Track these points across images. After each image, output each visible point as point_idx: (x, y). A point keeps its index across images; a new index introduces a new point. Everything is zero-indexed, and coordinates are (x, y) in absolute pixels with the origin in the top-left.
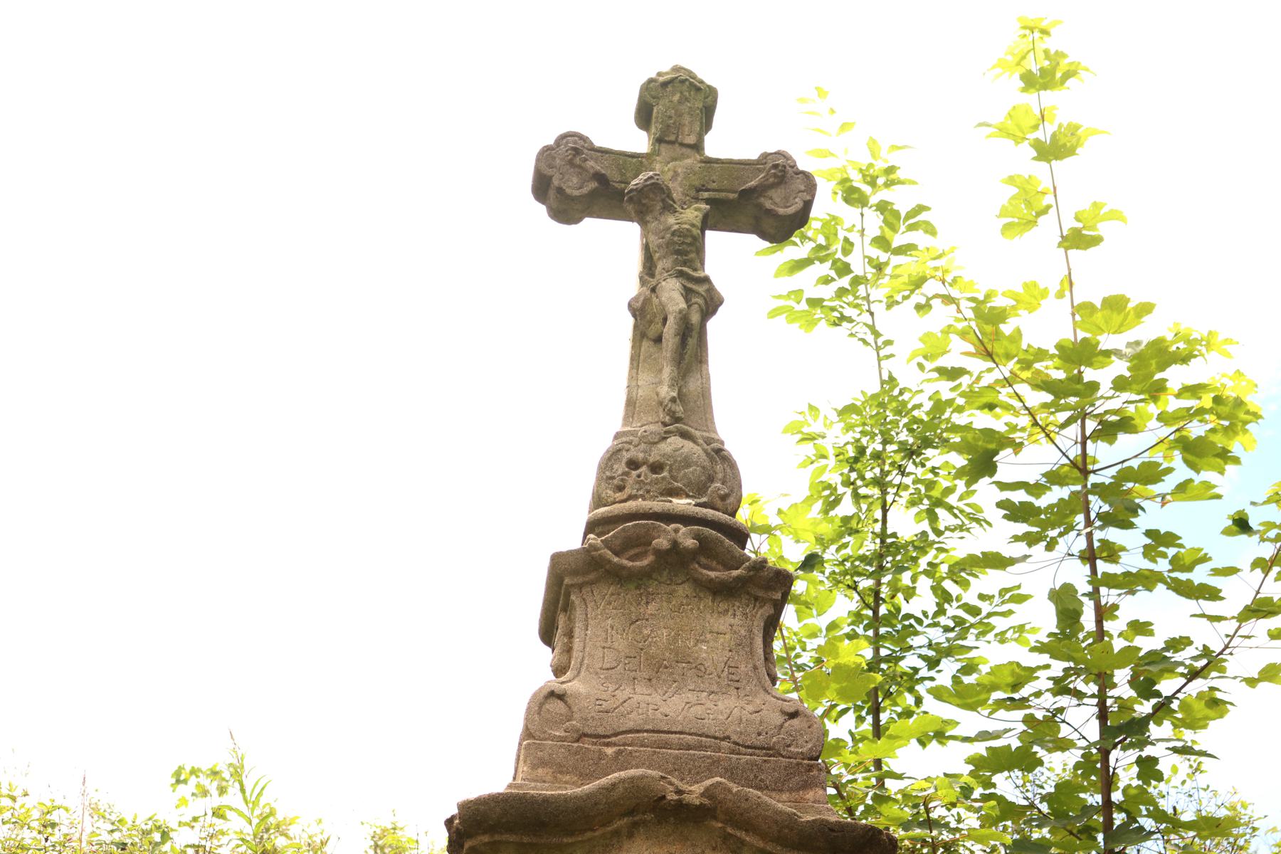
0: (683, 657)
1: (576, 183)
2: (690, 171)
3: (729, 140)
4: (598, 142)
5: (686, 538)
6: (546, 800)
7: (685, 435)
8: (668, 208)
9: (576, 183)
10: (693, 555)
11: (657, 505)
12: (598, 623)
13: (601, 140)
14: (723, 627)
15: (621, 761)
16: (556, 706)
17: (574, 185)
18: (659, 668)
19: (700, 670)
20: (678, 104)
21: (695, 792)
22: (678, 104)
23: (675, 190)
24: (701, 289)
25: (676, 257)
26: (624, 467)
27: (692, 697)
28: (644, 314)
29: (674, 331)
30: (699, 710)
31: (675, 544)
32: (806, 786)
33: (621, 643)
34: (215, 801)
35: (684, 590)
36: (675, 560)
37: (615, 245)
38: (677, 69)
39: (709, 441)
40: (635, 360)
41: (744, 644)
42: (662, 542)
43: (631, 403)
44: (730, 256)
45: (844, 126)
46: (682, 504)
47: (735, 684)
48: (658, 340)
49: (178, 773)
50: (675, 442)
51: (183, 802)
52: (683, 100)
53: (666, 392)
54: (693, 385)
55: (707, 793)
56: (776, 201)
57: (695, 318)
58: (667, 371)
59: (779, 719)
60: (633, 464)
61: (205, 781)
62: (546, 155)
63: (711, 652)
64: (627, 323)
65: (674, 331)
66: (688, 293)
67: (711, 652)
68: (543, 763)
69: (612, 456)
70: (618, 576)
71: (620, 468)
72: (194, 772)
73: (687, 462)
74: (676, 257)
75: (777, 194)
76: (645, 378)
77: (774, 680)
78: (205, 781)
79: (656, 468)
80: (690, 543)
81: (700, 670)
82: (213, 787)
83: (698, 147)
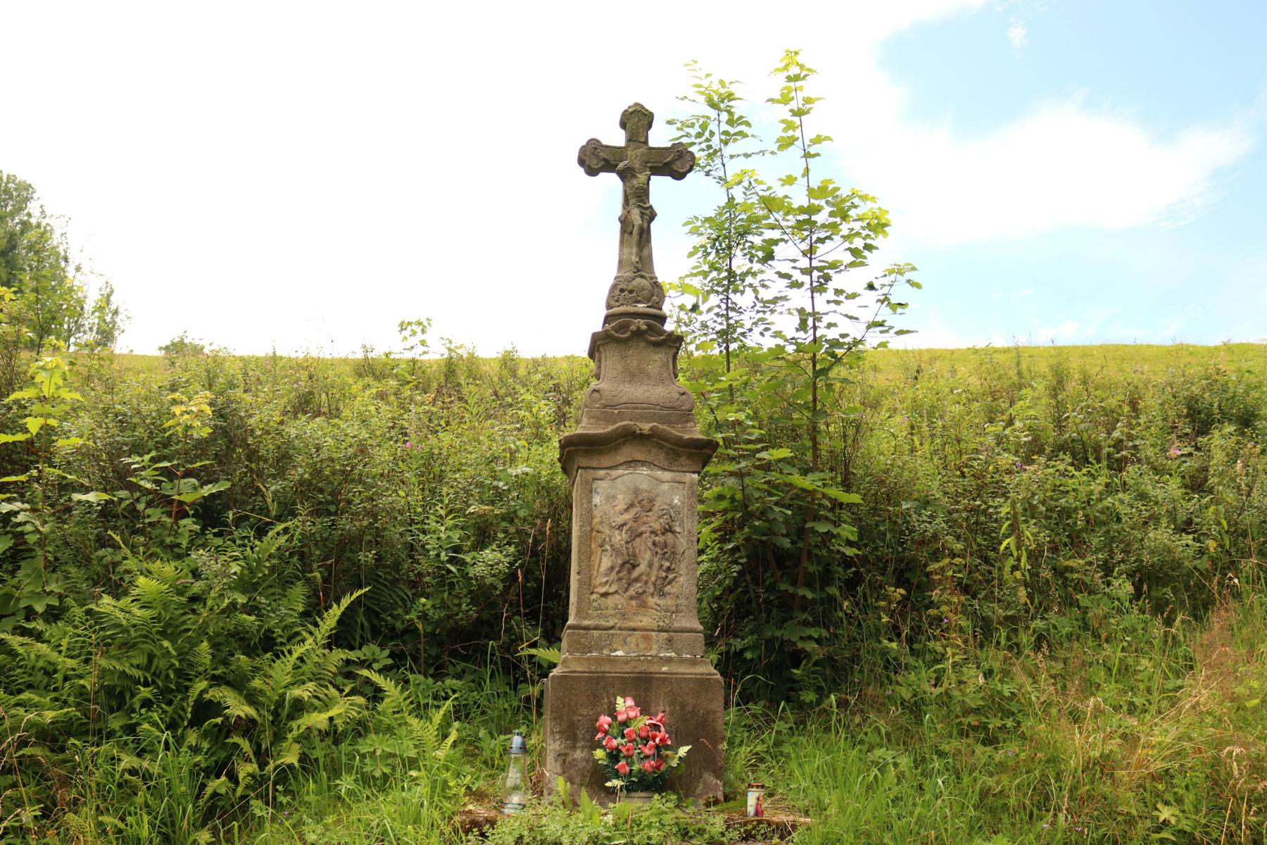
0: (642, 371)
1: (595, 159)
2: (643, 154)
3: (659, 137)
4: (604, 143)
5: (642, 324)
6: (594, 435)
7: (642, 277)
8: (634, 176)
9: (595, 159)
10: (646, 332)
11: (630, 309)
12: (612, 360)
13: (606, 141)
14: (658, 358)
15: (621, 417)
16: (596, 395)
17: (594, 164)
18: (633, 376)
19: (649, 377)
20: (637, 120)
21: (646, 427)
22: (637, 120)
23: (635, 159)
24: (647, 212)
25: (637, 198)
26: (619, 292)
27: (645, 388)
28: (625, 222)
29: (637, 229)
30: (647, 394)
31: (638, 328)
32: (687, 421)
33: (619, 367)
34: (420, 337)
35: (642, 344)
36: (639, 334)
37: (610, 184)
38: (637, 104)
39: (652, 278)
40: (622, 242)
41: (665, 365)
42: (633, 328)
43: (620, 262)
44: (660, 188)
45: (708, 75)
46: (641, 307)
47: (662, 381)
48: (631, 233)
49: (402, 324)
50: (638, 280)
51: (405, 338)
52: (640, 120)
53: (634, 258)
54: (645, 252)
55: (651, 429)
56: (677, 167)
57: (645, 226)
58: (635, 250)
59: (677, 396)
60: (622, 290)
61: (414, 327)
62: (583, 150)
63: (653, 369)
64: (618, 225)
65: (637, 229)
66: (642, 214)
67: (653, 369)
68: (592, 417)
69: (614, 287)
70: (618, 341)
71: (617, 292)
72: (410, 324)
73: (643, 289)
74: (637, 198)
75: (679, 163)
76: (626, 250)
77: (676, 376)
78: (414, 327)
79: (631, 292)
80: (644, 327)
81: (649, 377)
82: (418, 329)
83: (646, 142)
